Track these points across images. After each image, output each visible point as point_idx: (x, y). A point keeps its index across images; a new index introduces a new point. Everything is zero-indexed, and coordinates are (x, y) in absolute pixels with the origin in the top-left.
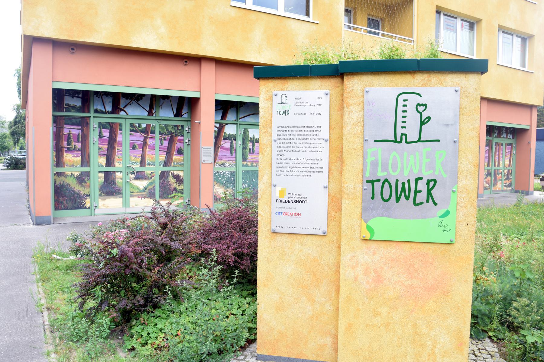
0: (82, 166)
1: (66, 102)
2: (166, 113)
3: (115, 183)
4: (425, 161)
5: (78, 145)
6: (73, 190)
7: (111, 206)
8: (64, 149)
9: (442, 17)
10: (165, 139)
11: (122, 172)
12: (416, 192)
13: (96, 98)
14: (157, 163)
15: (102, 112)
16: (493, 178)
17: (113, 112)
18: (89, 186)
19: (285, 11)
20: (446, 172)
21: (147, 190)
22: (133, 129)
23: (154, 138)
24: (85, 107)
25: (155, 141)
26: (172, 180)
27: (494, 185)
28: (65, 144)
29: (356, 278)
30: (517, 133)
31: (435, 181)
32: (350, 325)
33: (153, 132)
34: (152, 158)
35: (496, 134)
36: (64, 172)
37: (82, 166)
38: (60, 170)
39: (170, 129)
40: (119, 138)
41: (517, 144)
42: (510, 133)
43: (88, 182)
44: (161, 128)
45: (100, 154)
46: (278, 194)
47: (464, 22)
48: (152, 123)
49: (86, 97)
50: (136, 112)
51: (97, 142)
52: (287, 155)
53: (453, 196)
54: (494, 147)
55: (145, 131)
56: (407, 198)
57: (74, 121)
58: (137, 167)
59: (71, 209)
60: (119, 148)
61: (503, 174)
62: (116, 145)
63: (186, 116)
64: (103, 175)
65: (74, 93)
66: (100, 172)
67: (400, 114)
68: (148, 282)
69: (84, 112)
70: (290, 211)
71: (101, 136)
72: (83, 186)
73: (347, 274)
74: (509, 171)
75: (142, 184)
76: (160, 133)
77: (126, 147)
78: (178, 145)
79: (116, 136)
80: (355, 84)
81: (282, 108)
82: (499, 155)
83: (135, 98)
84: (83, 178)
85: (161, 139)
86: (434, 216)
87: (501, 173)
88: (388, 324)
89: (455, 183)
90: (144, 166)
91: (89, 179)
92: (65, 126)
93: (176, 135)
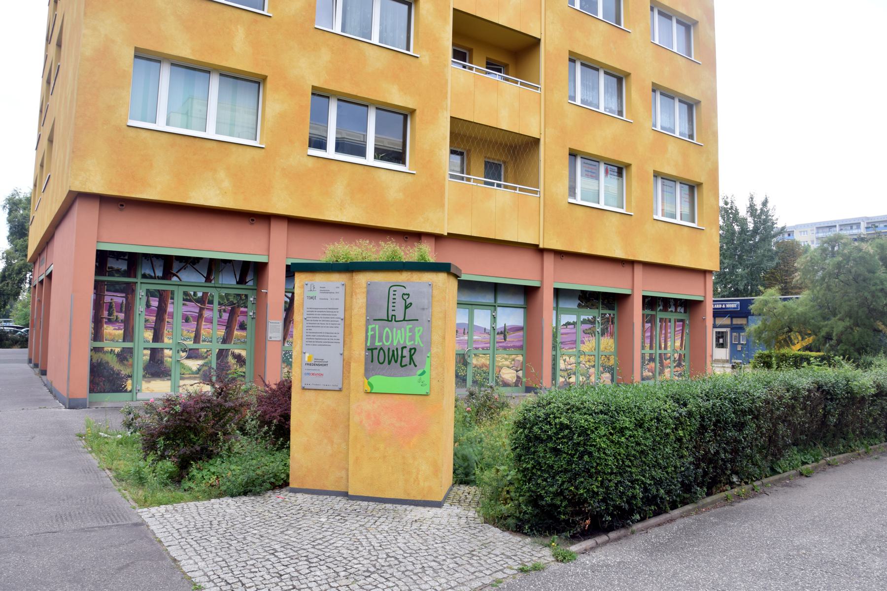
0: (124, 341)
1: (109, 265)
2: (228, 280)
3: (162, 362)
4: (408, 334)
5: (121, 316)
6: (112, 369)
7: (157, 390)
8: (105, 320)
9: (579, 161)
10: (225, 311)
11: (171, 349)
12: (402, 357)
13: (145, 261)
14: (214, 340)
15: (151, 277)
16: (658, 365)
17: (163, 278)
18: (132, 365)
19: (375, 158)
20: (423, 343)
21: (201, 372)
22: (187, 298)
23: (212, 310)
24: (131, 271)
25: (213, 313)
26: (231, 360)
27: (660, 374)
28: (106, 314)
29: (361, 422)
30: (690, 306)
31: (415, 349)
32: (357, 459)
33: (211, 302)
34: (208, 333)
35: (661, 307)
36: (103, 348)
37: (124, 341)
38: (98, 344)
39: (231, 299)
40: (170, 309)
41: (690, 319)
42: (681, 306)
43: (130, 360)
44: (221, 297)
45: (146, 327)
46: (306, 359)
47: (609, 167)
48: (210, 291)
49: (133, 260)
50: (191, 278)
51: (144, 313)
52: (314, 330)
53: (428, 360)
54: (658, 324)
55: (201, 301)
56: (396, 362)
57: (117, 287)
58: (190, 344)
59: (109, 392)
60: (170, 320)
61: (672, 359)
62: (166, 316)
63: (251, 283)
64: (148, 352)
65: (118, 255)
66: (145, 349)
67: (391, 300)
68: (203, 434)
69: (129, 276)
70: (316, 372)
71: (148, 305)
72: (124, 365)
73: (355, 419)
74: (680, 355)
75: (194, 364)
76: (220, 304)
77: (178, 319)
78: (240, 318)
79: (166, 306)
80: (363, 279)
81: (312, 294)
82: (666, 334)
83: (191, 262)
84: (125, 356)
85: (220, 311)
86: (415, 375)
87: (670, 358)
88: (385, 457)
89: (429, 350)
90: (199, 342)
91: (131, 357)
92: (106, 293)
93: (238, 307)
